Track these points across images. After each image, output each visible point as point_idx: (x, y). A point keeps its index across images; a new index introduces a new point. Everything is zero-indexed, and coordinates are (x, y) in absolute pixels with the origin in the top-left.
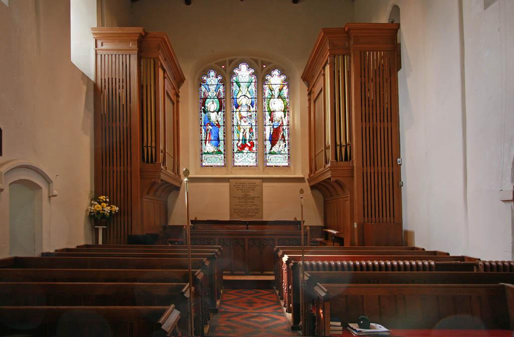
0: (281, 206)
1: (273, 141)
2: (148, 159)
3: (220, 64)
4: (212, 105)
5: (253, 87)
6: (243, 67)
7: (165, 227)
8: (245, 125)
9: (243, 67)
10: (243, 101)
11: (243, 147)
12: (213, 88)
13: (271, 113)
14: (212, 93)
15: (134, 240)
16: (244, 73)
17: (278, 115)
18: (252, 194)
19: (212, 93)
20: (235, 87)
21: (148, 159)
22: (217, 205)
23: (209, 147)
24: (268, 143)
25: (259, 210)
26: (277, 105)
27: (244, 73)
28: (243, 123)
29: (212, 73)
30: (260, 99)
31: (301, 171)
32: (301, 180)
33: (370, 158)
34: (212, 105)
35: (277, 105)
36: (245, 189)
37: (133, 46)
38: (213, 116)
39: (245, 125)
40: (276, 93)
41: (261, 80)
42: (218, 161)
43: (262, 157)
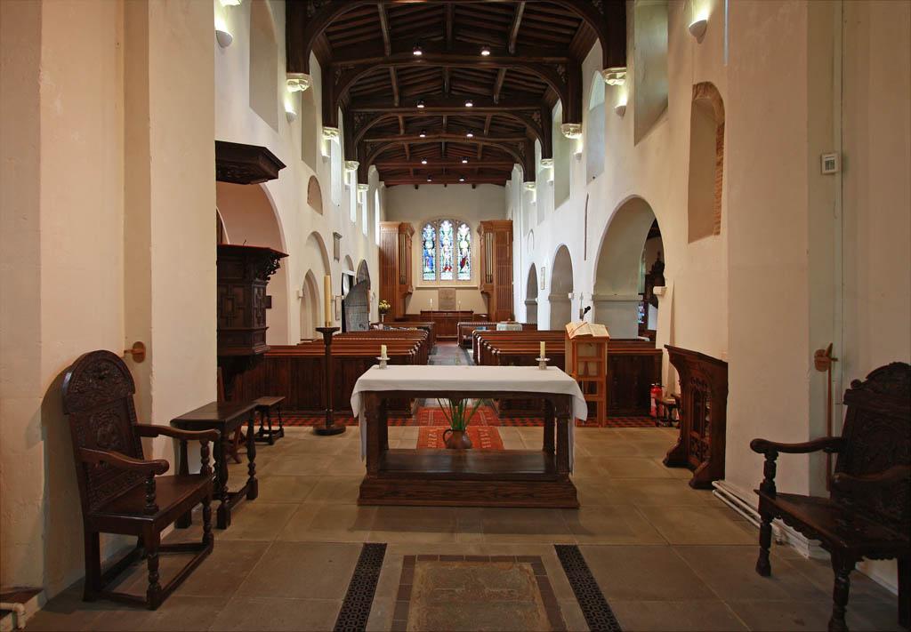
0: (464, 302)
1: (462, 265)
2: (385, 80)
3: (433, 222)
4: (429, 245)
5: (451, 234)
6: (446, 222)
7: (405, 315)
8: (447, 257)
9: (446, 222)
10: (445, 242)
11: (446, 269)
12: (429, 235)
13: (461, 249)
14: (429, 238)
15: (243, 287)
16: (446, 226)
17: (465, 250)
18: (451, 296)
19: (429, 238)
20: (442, 234)
21: (385, 80)
22: (431, 303)
23: (427, 269)
24: (459, 267)
25: (454, 305)
26: (464, 245)
27: (446, 226)
28: (446, 255)
29: (429, 226)
30: (455, 241)
31: (476, 284)
32: (476, 288)
33: (500, 282)
34: (429, 245)
35: (464, 245)
36: (447, 294)
37: (396, 229)
38: (430, 252)
39: (447, 257)
40: (463, 238)
41: (456, 231)
42: (432, 277)
43: (456, 276)
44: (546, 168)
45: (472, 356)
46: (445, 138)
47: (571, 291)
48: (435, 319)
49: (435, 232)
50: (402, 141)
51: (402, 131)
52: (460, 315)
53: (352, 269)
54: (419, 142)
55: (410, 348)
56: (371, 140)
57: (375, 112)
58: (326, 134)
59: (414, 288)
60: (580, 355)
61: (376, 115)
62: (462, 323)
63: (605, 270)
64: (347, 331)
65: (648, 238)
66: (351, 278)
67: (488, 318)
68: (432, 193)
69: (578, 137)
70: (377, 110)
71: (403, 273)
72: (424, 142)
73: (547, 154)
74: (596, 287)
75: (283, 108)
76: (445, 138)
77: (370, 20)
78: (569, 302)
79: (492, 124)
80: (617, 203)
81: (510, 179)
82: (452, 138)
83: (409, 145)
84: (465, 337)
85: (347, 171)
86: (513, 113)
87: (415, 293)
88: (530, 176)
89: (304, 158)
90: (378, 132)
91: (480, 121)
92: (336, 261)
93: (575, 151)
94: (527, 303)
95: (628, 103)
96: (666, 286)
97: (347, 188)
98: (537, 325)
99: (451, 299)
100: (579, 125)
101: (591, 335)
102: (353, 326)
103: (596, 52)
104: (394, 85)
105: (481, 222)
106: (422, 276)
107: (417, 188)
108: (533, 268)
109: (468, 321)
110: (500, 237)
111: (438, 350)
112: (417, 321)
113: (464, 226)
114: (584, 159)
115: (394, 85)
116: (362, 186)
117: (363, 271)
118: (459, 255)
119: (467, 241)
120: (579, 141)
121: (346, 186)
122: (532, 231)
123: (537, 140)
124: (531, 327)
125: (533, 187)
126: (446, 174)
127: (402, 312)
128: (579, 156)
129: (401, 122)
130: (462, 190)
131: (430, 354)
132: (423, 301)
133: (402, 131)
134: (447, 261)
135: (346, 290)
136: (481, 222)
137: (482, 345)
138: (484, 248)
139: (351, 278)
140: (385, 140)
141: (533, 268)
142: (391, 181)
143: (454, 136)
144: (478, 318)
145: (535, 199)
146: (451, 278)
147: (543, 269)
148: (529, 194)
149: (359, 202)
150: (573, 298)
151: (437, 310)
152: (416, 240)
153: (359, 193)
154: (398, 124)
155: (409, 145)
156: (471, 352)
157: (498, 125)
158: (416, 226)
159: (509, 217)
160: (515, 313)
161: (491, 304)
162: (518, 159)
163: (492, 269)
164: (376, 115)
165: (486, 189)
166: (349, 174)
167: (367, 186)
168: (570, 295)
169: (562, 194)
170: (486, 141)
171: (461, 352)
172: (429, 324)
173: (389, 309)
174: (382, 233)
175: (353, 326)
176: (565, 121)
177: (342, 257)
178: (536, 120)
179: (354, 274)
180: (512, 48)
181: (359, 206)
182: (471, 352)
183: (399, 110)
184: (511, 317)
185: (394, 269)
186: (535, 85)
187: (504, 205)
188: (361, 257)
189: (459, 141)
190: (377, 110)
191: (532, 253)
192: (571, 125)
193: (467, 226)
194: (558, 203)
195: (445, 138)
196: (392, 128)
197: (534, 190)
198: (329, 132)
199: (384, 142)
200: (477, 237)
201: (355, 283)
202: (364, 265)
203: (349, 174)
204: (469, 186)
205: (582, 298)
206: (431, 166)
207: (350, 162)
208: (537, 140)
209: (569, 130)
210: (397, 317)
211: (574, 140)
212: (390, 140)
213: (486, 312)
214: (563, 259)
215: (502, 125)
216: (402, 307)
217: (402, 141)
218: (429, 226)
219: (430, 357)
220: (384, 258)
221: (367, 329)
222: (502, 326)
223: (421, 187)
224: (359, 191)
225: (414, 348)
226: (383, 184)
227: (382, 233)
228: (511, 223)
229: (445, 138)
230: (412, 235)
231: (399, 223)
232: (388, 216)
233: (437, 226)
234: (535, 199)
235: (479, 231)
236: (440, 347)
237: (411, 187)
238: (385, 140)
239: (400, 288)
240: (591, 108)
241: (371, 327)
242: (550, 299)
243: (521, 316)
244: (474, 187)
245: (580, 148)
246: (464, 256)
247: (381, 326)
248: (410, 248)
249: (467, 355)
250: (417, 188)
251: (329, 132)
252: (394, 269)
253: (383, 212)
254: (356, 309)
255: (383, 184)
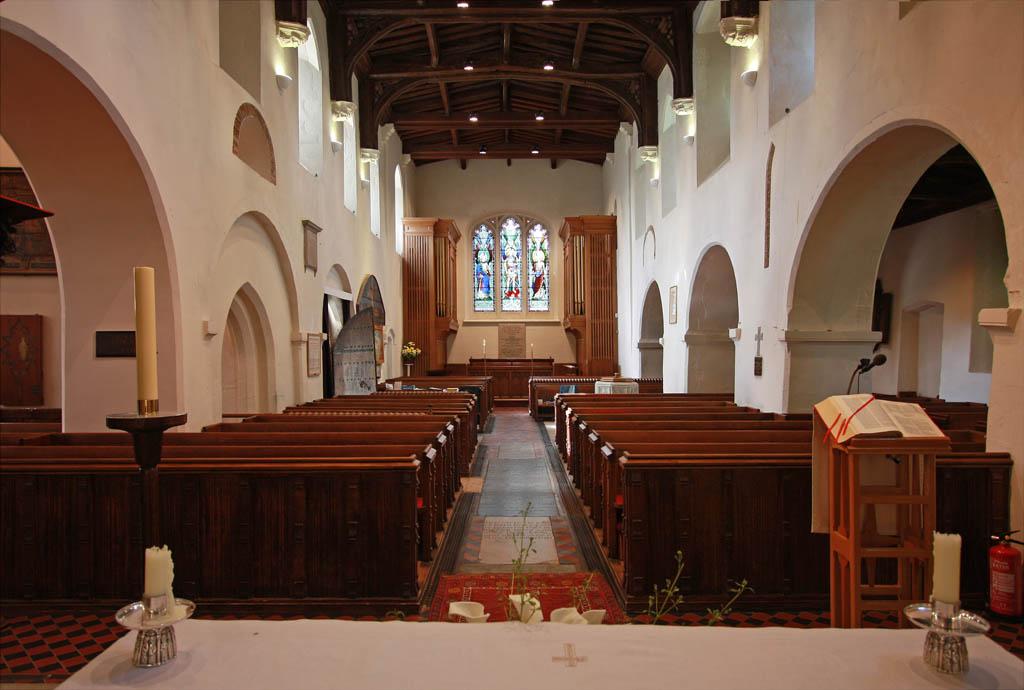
1: (536, 290)
4: (483, 256)
5: (518, 241)
7: (446, 365)
11: (510, 293)
12: (484, 241)
13: (534, 263)
14: (484, 246)
16: (511, 228)
17: (540, 265)
18: (517, 336)
20: (503, 241)
23: (481, 294)
24: (531, 291)
25: (523, 349)
26: (539, 256)
27: (511, 228)
28: (511, 273)
29: (484, 228)
30: (525, 251)
31: (558, 316)
33: (596, 314)
34: (483, 256)
35: (539, 256)
36: (512, 333)
37: (430, 230)
38: (485, 267)
39: (512, 275)
40: (538, 245)
41: (525, 234)
42: (488, 306)
43: (526, 303)
44: (679, 117)
45: (553, 437)
46: (506, 72)
47: (734, 323)
48: (493, 372)
49: (493, 236)
50: (436, 77)
51: (435, 60)
52: (533, 365)
53: (348, 289)
54: (462, 80)
55: (447, 420)
56: (381, 76)
57: (385, 17)
58: (283, 35)
59: (460, 323)
60: (864, 482)
61: (387, 21)
62: (536, 379)
63: (810, 285)
64: (338, 392)
65: (893, 228)
66: (346, 304)
67: (577, 372)
68: (486, 169)
69: (750, 43)
70: (390, 12)
71: (441, 299)
72: (471, 79)
73: (684, 89)
74: (792, 317)
75: (271, 69)
76: (508, 73)
77: (417, 38)
78: (730, 345)
79: (586, 49)
80: (851, 146)
81: (612, 151)
82: (520, 75)
83: (448, 85)
84: (540, 401)
85: (335, 119)
86: (624, 18)
87: (461, 330)
88: (649, 136)
89: (227, 63)
90: (396, 61)
91: (562, 43)
92: (310, 273)
93: (686, 134)
94: (642, 347)
95: (761, 68)
96: (400, 355)
97: (336, 150)
98: (661, 382)
99: (518, 339)
100: (752, 20)
101: (899, 434)
102: (349, 385)
103: (666, 79)
104: (432, 42)
105: (567, 219)
106: (473, 305)
107: (464, 167)
108: (654, 292)
109: (546, 374)
110: (594, 244)
111: (497, 424)
112: (463, 374)
113: (538, 227)
114: (764, 85)
115: (432, 42)
116: (368, 151)
117: (370, 294)
118: (531, 272)
119: (544, 251)
120: (751, 49)
121: (363, 182)
122: (651, 228)
123: (667, 68)
124: (651, 385)
125: (654, 155)
126: (510, 143)
127: (440, 361)
128: (753, 76)
129: (454, 136)
130: (534, 170)
131: (481, 432)
132: (475, 344)
133: (435, 60)
134: (511, 283)
135: (336, 323)
136: (567, 219)
137: (575, 426)
138: (570, 260)
139: (346, 304)
140: (405, 75)
141: (654, 292)
142: (424, 154)
143: (522, 69)
144: (561, 369)
145: (657, 174)
146: (518, 308)
147: (674, 289)
148: (646, 168)
149: (363, 178)
150: (739, 336)
151: (496, 357)
152: (463, 247)
153: (360, 169)
154: (428, 48)
155: (448, 85)
156: (552, 427)
157: (598, 51)
158: (462, 227)
159: (610, 212)
160: (620, 364)
161: (582, 348)
162: (630, 110)
163: (584, 294)
164: (387, 21)
165: (572, 168)
166: (341, 125)
167: (375, 153)
168: (732, 333)
169: (713, 153)
170: (575, 79)
171: (531, 426)
172: (481, 381)
173: (418, 355)
174: (404, 235)
175: (349, 385)
176: (677, 95)
177: (325, 264)
178: (664, 31)
179: (353, 297)
180: (563, 110)
181: (363, 187)
182: (552, 427)
183: (426, 11)
184: (612, 369)
185: (427, 295)
186: (629, 44)
187: (602, 194)
188: (367, 270)
189: (531, 79)
190: (390, 12)
191: (656, 261)
192: (737, 19)
193: (543, 227)
194: (703, 174)
195: (508, 73)
196: (416, 56)
197: (656, 161)
198: (288, 32)
199: (405, 79)
200: (558, 243)
201: (354, 311)
202: (372, 284)
203: (341, 125)
204: (546, 162)
205: (759, 337)
206: (479, 73)
207: (339, 103)
208: (667, 68)
209: (735, 30)
210: (432, 368)
211: (741, 50)
212: (415, 74)
213: (574, 361)
214: (715, 273)
215: (606, 52)
216: (440, 350)
217: (436, 77)
218: (484, 228)
219: (480, 438)
220: (410, 275)
221: (374, 390)
222: (603, 386)
223: (472, 163)
224: (363, 161)
225: (469, 402)
226: (408, 158)
227: (404, 235)
228: (613, 220)
229: (506, 72)
230: (456, 241)
231: (434, 219)
232: (417, 208)
233: (496, 232)
234: (657, 174)
235: (562, 235)
236: (499, 417)
237: (453, 165)
238: (405, 75)
239: (436, 321)
240: (664, 130)
241: (381, 388)
242: (688, 339)
243: (631, 365)
244: (554, 166)
245: (753, 64)
246: (538, 274)
247: (399, 385)
248: (454, 261)
249: (544, 432)
250: (464, 167)
251: (288, 32)
252: (427, 295)
253: (409, 206)
254: (355, 357)
255: (408, 158)
